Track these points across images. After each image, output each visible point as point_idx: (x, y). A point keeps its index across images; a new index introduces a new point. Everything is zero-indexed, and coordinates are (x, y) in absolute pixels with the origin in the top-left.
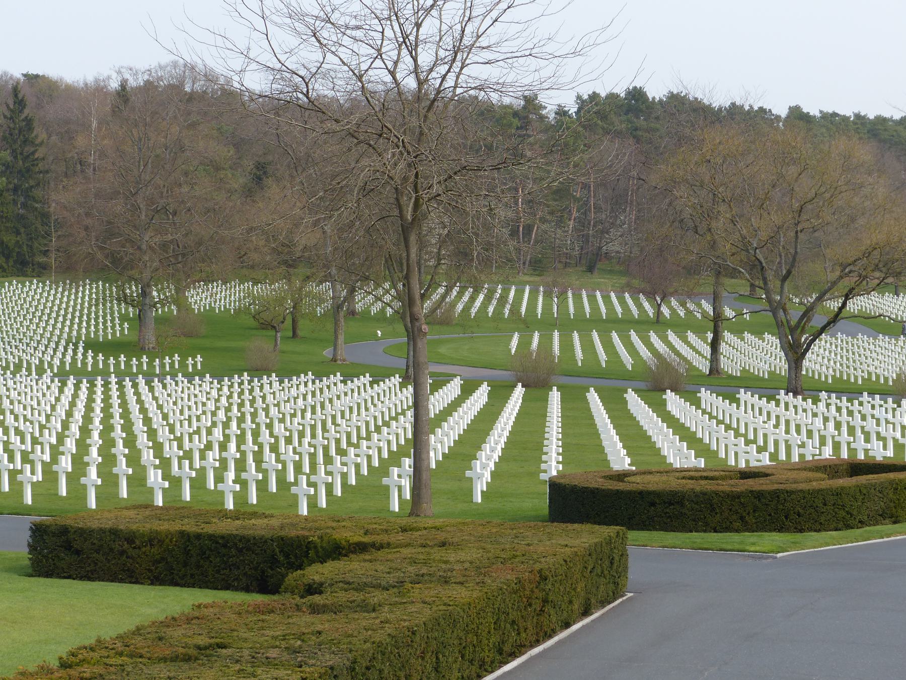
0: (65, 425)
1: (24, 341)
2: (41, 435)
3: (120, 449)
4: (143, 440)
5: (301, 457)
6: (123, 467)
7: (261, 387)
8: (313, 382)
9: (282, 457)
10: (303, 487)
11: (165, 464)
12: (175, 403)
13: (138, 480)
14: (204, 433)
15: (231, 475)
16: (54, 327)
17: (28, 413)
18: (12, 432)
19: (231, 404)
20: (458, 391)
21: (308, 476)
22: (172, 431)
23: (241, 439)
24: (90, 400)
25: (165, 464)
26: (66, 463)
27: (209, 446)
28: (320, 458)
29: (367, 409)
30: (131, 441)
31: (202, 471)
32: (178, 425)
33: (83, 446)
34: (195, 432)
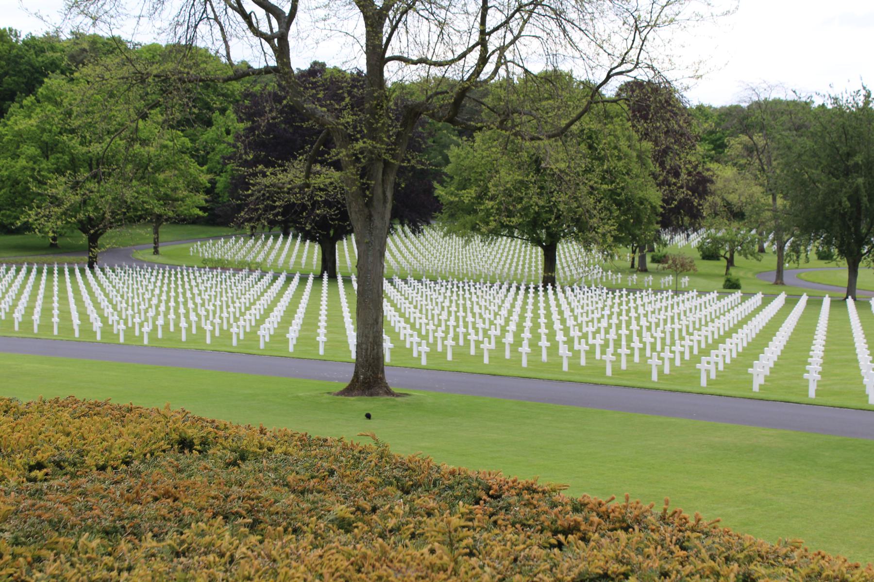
0: (510, 313)
1: (484, 259)
2: (495, 319)
3: (542, 320)
4: (555, 316)
5: (663, 362)
6: (544, 343)
7: (635, 300)
8: (673, 297)
9: (644, 340)
10: (654, 361)
11: (570, 342)
12: (579, 301)
13: (554, 348)
14: (596, 321)
15: (611, 349)
16: (503, 250)
17: (487, 304)
18: (477, 316)
19: (614, 304)
20: (759, 303)
21: (659, 353)
22: (576, 319)
23: (619, 327)
24: (524, 309)
25: (570, 342)
26: (509, 339)
27: (598, 331)
28: (668, 341)
29: (706, 308)
30: (550, 325)
31: (593, 347)
32: (579, 316)
33: (520, 327)
34: (590, 321)
